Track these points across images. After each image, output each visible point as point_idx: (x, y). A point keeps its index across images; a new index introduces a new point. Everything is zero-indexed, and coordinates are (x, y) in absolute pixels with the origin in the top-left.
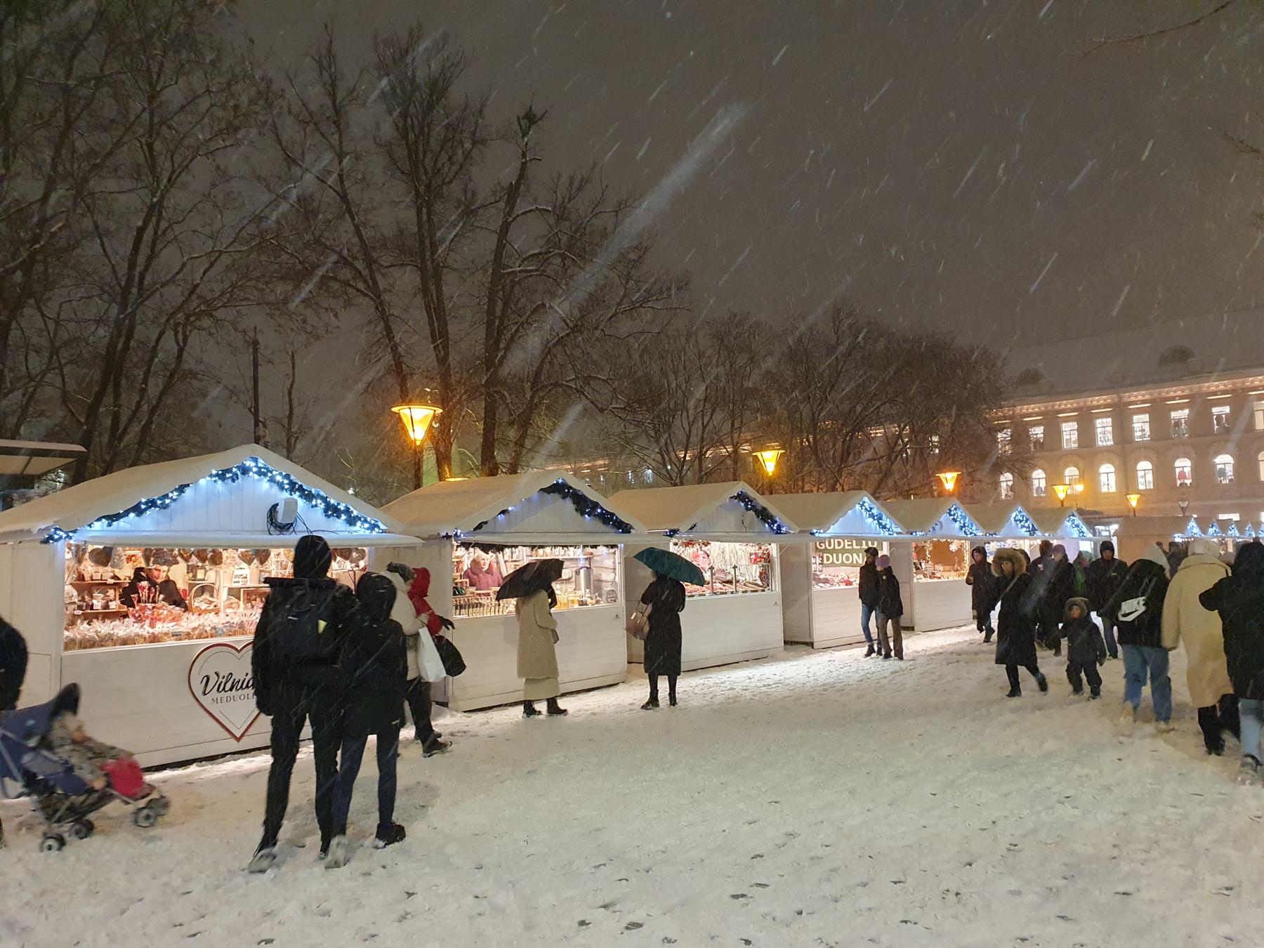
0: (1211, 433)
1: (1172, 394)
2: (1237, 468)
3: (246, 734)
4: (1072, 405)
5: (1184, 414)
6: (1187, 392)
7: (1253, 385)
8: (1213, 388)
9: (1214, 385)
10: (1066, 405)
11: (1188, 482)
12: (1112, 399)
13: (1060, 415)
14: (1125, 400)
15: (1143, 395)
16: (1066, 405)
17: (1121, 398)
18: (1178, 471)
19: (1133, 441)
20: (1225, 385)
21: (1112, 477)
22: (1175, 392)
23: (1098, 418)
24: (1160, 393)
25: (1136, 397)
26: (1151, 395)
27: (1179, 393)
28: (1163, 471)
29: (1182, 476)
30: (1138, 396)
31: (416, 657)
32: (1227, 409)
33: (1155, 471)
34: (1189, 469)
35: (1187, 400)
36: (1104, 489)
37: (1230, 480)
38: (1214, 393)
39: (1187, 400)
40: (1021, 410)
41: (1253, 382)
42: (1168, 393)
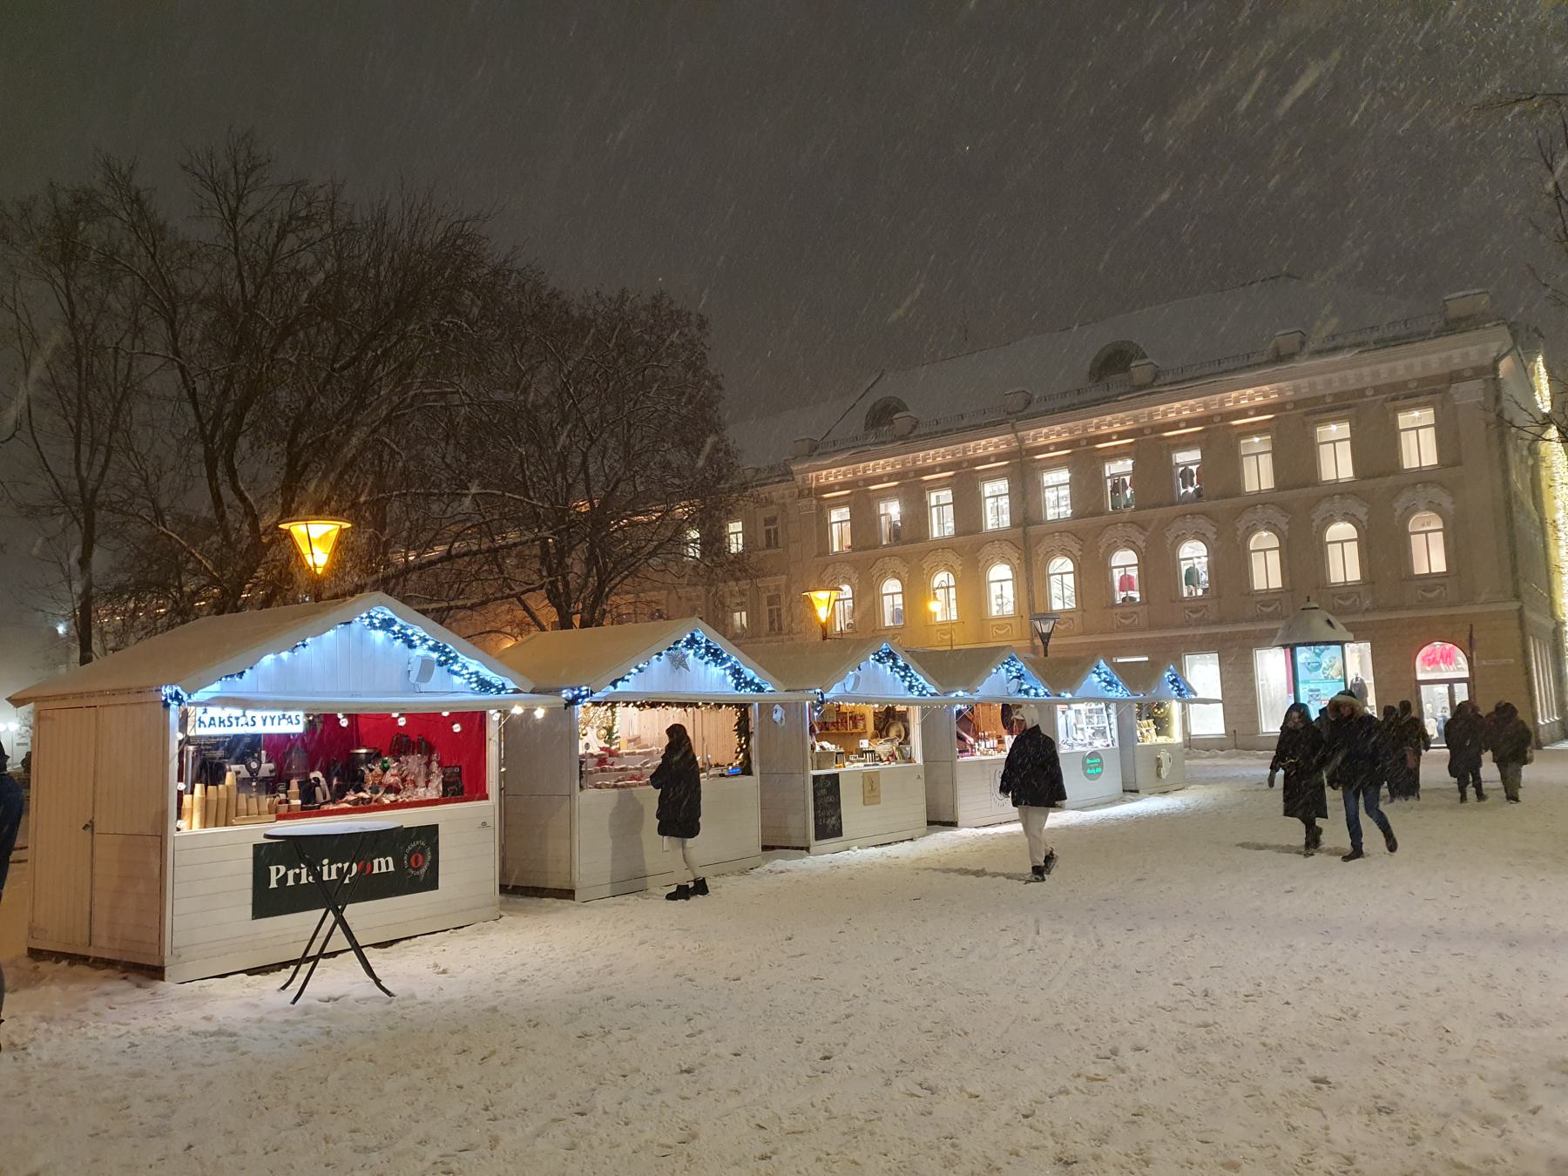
0: (878, 545)
1: (1105, 430)
2: (1213, 569)
3: (308, 942)
4: (944, 457)
5: (1123, 466)
6: (1129, 425)
7: (1238, 407)
8: (1172, 416)
9: (1178, 409)
10: (985, 448)
11: (1136, 595)
12: (1008, 443)
13: (926, 478)
14: (1029, 443)
15: (1059, 434)
16: (985, 448)
17: (1021, 441)
18: (1184, 567)
19: (1041, 521)
20: (1265, 395)
21: (1009, 589)
22: (1112, 423)
23: (931, 489)
24: (1085, 429)
25: (1047, 436)
26: (1071, 431)
27: (1117, 427)
28: (1092, 574)
29: (1191, 576)
30: (1047, 435)
31: (1288, 849)
32: (1195, 455)
33: (1078, 573)
34: (1205, 560)
35: (951, 473)
36: (994, 611)
37: (1205, 591)
38: (1174, 425)
39: (951, 473)
40: (865, 471)
41: (1237, 401)
42: (1098, 427)
